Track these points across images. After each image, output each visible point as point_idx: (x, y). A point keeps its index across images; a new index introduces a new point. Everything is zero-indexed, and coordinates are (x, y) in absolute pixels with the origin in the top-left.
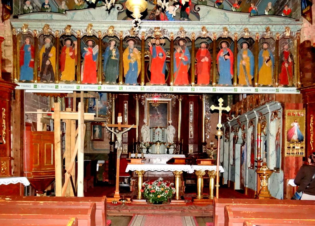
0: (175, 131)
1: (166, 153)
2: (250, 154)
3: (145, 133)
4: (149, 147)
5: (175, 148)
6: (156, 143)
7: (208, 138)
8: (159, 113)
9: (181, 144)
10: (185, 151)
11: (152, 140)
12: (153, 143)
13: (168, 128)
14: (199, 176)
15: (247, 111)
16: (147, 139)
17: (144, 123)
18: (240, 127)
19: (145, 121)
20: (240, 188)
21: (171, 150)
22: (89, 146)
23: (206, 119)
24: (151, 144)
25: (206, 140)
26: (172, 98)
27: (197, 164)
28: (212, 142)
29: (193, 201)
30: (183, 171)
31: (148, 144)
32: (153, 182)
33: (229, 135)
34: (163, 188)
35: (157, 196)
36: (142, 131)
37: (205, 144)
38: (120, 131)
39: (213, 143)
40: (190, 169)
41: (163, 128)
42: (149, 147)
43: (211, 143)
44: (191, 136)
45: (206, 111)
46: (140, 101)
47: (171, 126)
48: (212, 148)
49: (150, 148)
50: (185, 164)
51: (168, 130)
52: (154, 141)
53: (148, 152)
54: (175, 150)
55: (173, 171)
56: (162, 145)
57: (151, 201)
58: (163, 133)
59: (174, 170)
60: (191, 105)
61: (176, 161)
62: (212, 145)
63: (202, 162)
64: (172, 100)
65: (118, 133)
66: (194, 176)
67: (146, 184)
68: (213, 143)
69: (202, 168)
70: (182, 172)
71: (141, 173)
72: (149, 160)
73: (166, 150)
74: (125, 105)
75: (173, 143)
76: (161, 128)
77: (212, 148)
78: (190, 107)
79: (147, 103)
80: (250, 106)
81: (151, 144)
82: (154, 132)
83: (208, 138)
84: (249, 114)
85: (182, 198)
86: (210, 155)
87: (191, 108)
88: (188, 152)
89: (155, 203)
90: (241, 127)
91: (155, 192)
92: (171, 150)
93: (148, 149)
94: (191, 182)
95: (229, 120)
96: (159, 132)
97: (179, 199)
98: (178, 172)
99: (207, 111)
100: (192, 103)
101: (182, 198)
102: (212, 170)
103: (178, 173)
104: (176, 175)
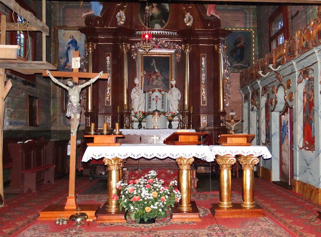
0: (180, 95)
1: (168, 128)
2: (302, 125)
3: (137, 99)
4: (142, 119)
5: (180, 121)
6: (153, 113)
7: (227, 105)
8: (157, 71)
9: (189, 115)
10: (194, 122)
11: (148, 110)
12: (149, 113)
13: (170, 92)
14: (224, 166)
15: (295, 56)
16: (140, 107)
17: (135, 85)
18: (281, 85)
19: (137, 81)
20: (280, 178)
21: (175, 124)
22: (60, 121)
23: (224, 79)
24: (145, 114)
25: (225, 108)
26: (175, 49)
27: (218, 144)
28: (232, 111)
29: (213, 213)
30: (194, 157)
31: (141, 114)
32: (138, 179)
33: (259, 100)
34: (155, 192)
35: (144, 209)
36: (132, 96)
37: (224, 113)
38: (76, 84)
39: (233, 114)
40: (208, 153)
41: (163, 91)
42: (142, 119)
43: (231, 114)
44: (204, 103)
45: (225, 68)
46: (130, 53)
47: (174, 88)
48: (233, 121)
49: (143, 120)
50: (199, 144)
51: (170, 94)
52: (151, 110)
53: (140, 127)
54: (181, 123)
55: (174, 158)
56: (162, 116)
57: (133, 217)
58: (163, 99)
59: (178, 157)
60: (203, 59)
61: (181, 138)
62: (232, 116)
63: (229, 140)
64: (176, 52)
65: (72, 87)
66: (215, 167)
67: (122, 185)
68: (233, 114)
69: (228, 151)
70: (193, 160)
71: (114, 162)
72: (141, 139)
73: (168, 123)
74: (108, 58)
75: (178, 112)
76: (160, 91)
77: (233, 121)
78: (202, 61)
79: (139, 56)
80: (302, 47)
81: (145, 114)
82: (150, 98)
83: (227, 105)
84: (298, 62)
85: (194, 207)
86: (231, 130)
87: (203, 63)
88: (200, 126)
89: (142, 221)
90: (282, 85)
91: (141, 200)
92: (175, 124)
93: (140, 122)
94: (205, 169)
95: (262, 75)
96: (157, 97)
97: (189, 212)
98: (185, 159)
99: (225, 68)
100: (204, 56)
101: (194, 207)
102: (249, 154)
103: (185, 161)
104: (181, 164)
